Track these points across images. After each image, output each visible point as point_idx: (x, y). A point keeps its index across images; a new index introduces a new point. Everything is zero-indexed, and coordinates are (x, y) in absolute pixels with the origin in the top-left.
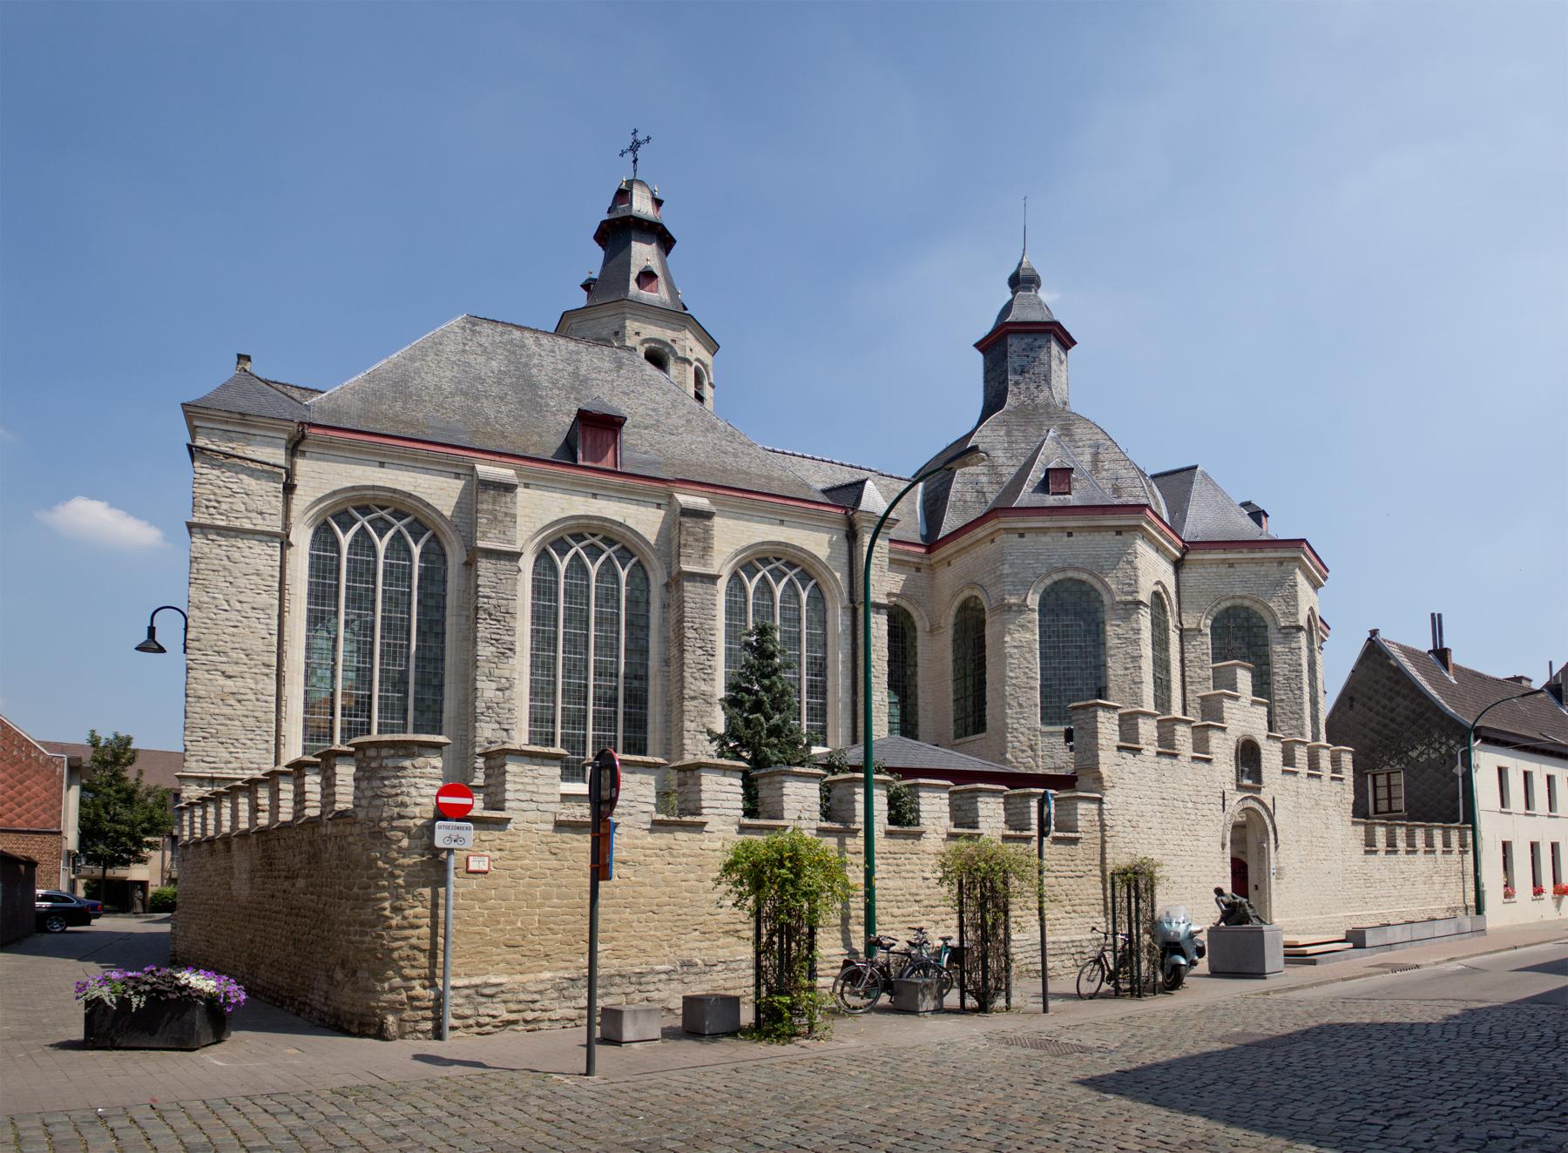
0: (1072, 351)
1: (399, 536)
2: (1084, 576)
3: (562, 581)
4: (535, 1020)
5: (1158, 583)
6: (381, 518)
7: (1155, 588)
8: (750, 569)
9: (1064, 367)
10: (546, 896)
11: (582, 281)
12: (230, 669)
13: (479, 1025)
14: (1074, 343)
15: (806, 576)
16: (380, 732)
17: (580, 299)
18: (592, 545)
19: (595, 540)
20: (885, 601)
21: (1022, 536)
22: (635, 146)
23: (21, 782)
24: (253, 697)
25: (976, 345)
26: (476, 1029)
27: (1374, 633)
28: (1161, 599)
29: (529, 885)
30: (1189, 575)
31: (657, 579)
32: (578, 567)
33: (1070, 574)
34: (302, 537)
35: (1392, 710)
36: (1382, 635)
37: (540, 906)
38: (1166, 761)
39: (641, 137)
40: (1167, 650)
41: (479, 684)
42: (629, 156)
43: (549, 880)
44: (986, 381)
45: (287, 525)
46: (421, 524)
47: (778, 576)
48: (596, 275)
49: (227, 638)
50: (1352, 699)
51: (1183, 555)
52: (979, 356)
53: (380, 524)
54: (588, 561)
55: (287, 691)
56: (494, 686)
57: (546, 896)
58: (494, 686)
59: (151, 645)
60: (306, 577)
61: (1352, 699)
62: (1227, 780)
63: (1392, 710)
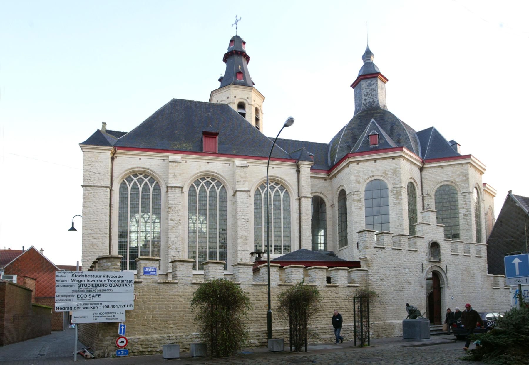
0: (388, 83)
1: (146, 184)
2: (381, 178)
3: (198, 195)
4: (151, 351)
5: (411, 178)
6: (141, 178)
7: (410, 180)
8: (197, 183)
9: (383, 91)
10: (154, 308)
11: (218, 78)
12: (95, 236)
13: (133, 352)
14: (387, 80)
15: (282, 188)
16: (141, 255)
17: (219, 84)
18: (208, 181)
19: (209, 180)
20: (310, 196)
21: (358, 163)
22: (236, 23)
23: (51, 280)
24: (101, 245)
25: (351, 86)
26: (132, 354)
27: (510, 192)
28: (413, 185)
29: (148, 304)
30: (425, 173)
31: (230, 193)
32: (203, 190)
33: (376, 177)
34: (116, 187)
35: (517, 226)
36: (513, 193)
37: (152, 311)
38: (396, 252)
39: (238, 18)
40: (415, 206)
41: (169, 236)
42: (235, 26)
43: (155, 302)
44: (355, 100)
45: (112, 183)
46: (153, 179)
47: (273, 188)
48: (223, 75)
49: (94, 225)
50: (501, 221)
51: (423, 165)
52: (353, 90)
53: (140, 180)
54: (206, 187)
55: (112, 242)
56: (174, 236)
57: (154, 308)
58: (174, 236)
59: (73, 229)
60: (118, 201)
61: (501, 221)
62: (424, 259)
63: (517, 226)
